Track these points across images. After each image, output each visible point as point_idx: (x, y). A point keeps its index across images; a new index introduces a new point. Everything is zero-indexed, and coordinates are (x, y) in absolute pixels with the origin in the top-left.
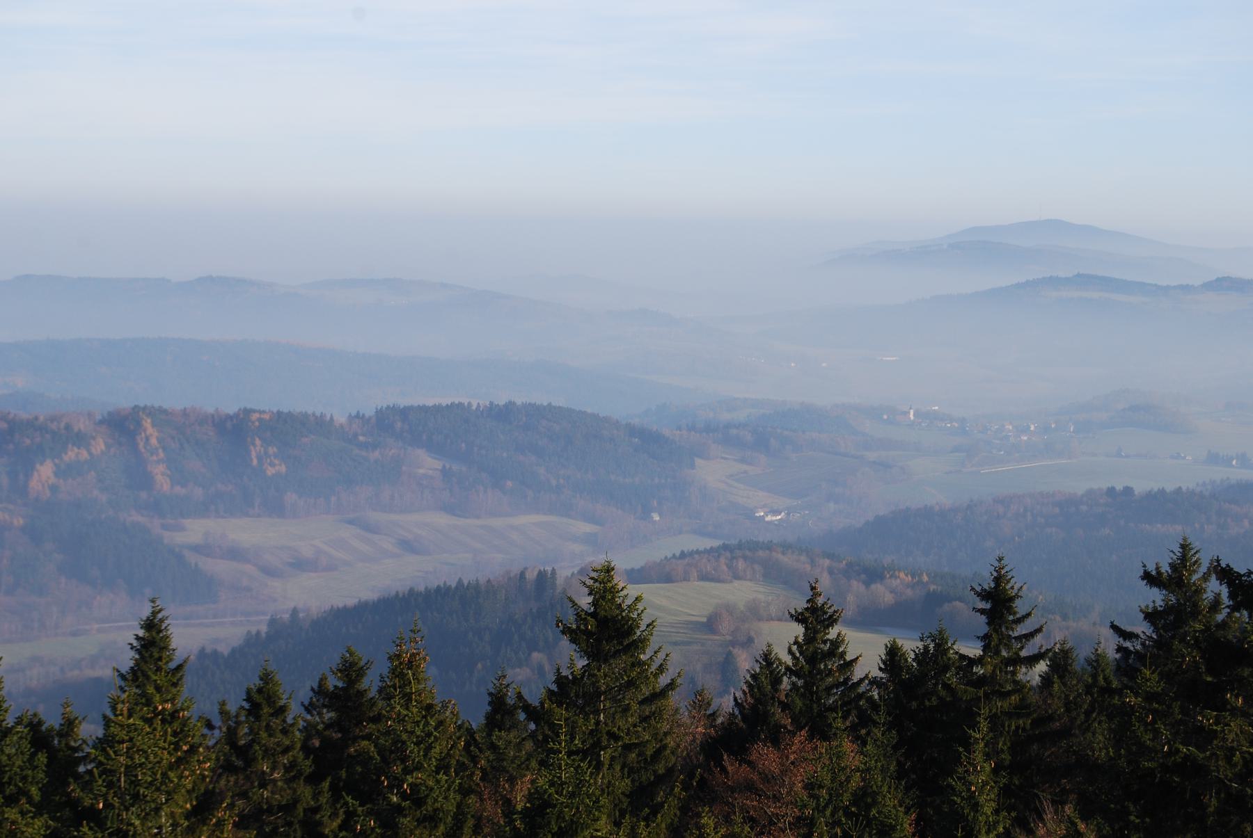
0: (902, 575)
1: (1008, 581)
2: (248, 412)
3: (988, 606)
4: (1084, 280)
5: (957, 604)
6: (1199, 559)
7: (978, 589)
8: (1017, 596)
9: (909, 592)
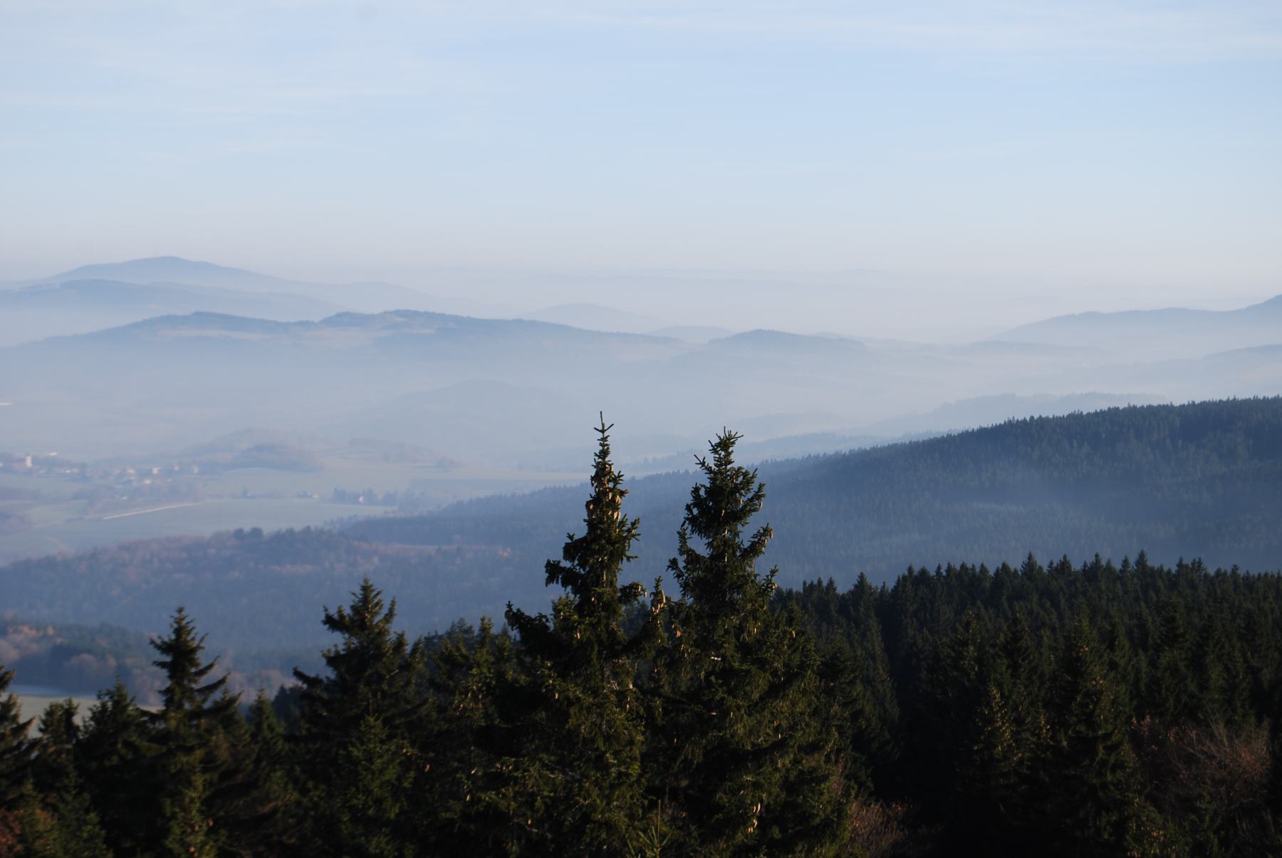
0: (26, 629)
1: (189, 632)
2: (308, 528)
3: (168, 659)
4: (202, 319)
5: (85, 656)
6: (380, 601)
7: (159, 642)
8: (199, 647)
9: (34, 647)
